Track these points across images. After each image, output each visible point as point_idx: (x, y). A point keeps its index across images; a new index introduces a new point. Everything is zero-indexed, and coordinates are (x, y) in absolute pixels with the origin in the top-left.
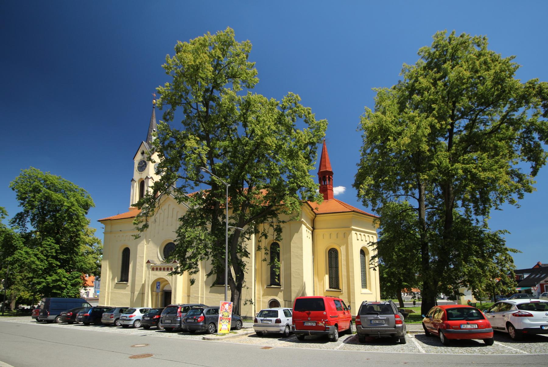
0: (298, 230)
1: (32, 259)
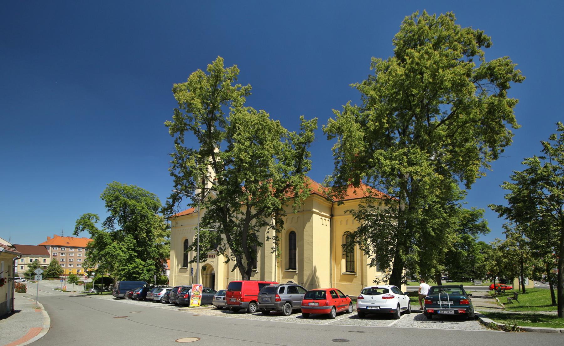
1: (118, 252)
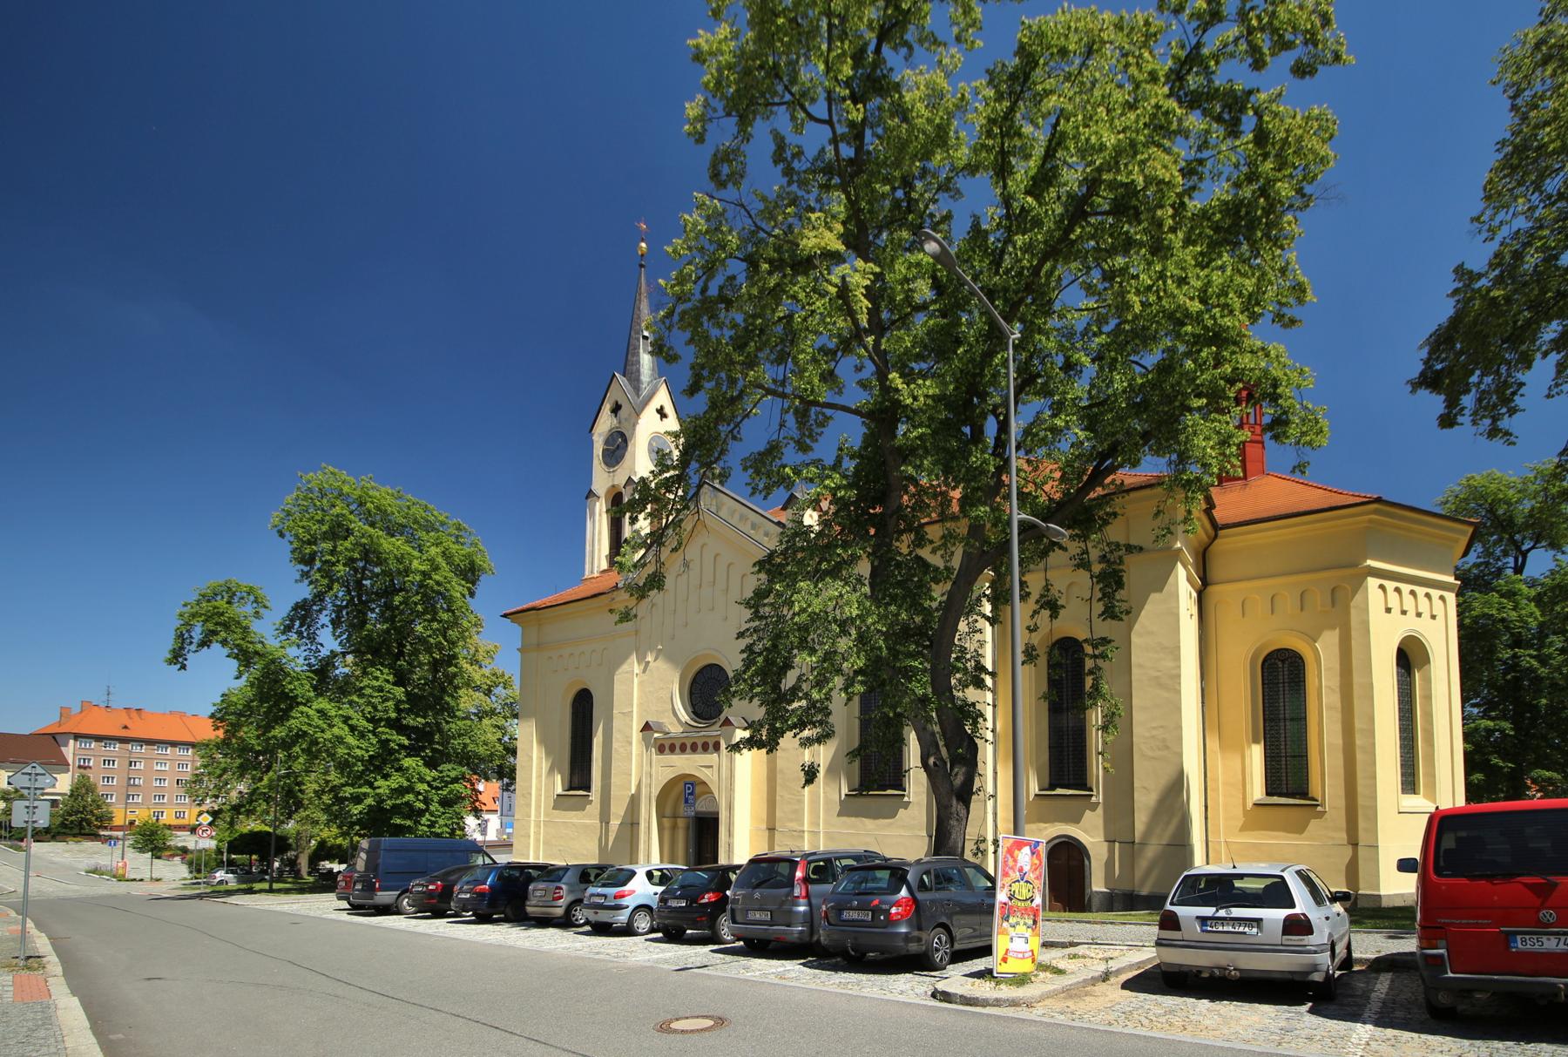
0: (1160, 581)
1: (336, 730)
